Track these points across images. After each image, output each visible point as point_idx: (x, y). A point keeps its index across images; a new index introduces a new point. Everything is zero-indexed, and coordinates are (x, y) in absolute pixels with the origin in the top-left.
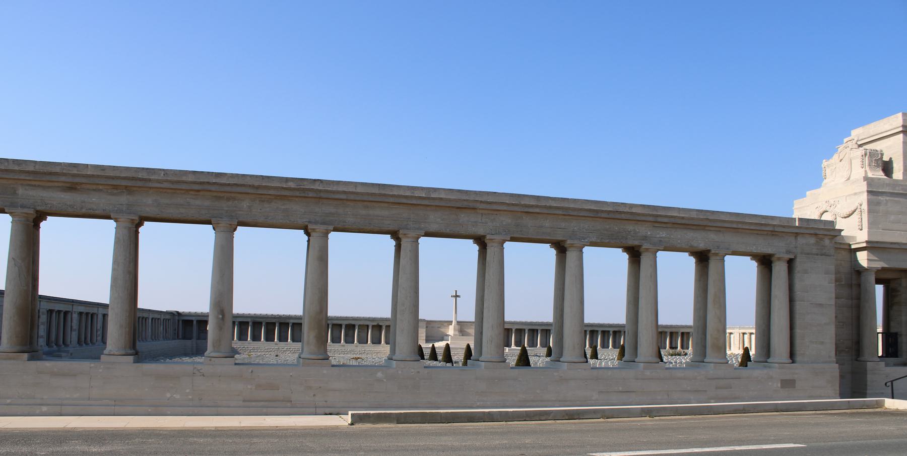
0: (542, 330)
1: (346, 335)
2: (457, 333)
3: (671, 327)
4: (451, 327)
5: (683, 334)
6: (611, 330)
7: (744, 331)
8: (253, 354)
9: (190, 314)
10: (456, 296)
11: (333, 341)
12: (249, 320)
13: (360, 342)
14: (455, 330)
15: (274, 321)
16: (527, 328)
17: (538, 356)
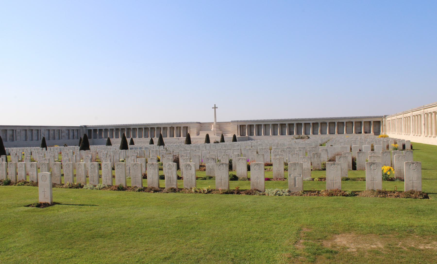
5: (177, 127)
9: (90, 127)
12: (113, 128)
14: (214, 127)
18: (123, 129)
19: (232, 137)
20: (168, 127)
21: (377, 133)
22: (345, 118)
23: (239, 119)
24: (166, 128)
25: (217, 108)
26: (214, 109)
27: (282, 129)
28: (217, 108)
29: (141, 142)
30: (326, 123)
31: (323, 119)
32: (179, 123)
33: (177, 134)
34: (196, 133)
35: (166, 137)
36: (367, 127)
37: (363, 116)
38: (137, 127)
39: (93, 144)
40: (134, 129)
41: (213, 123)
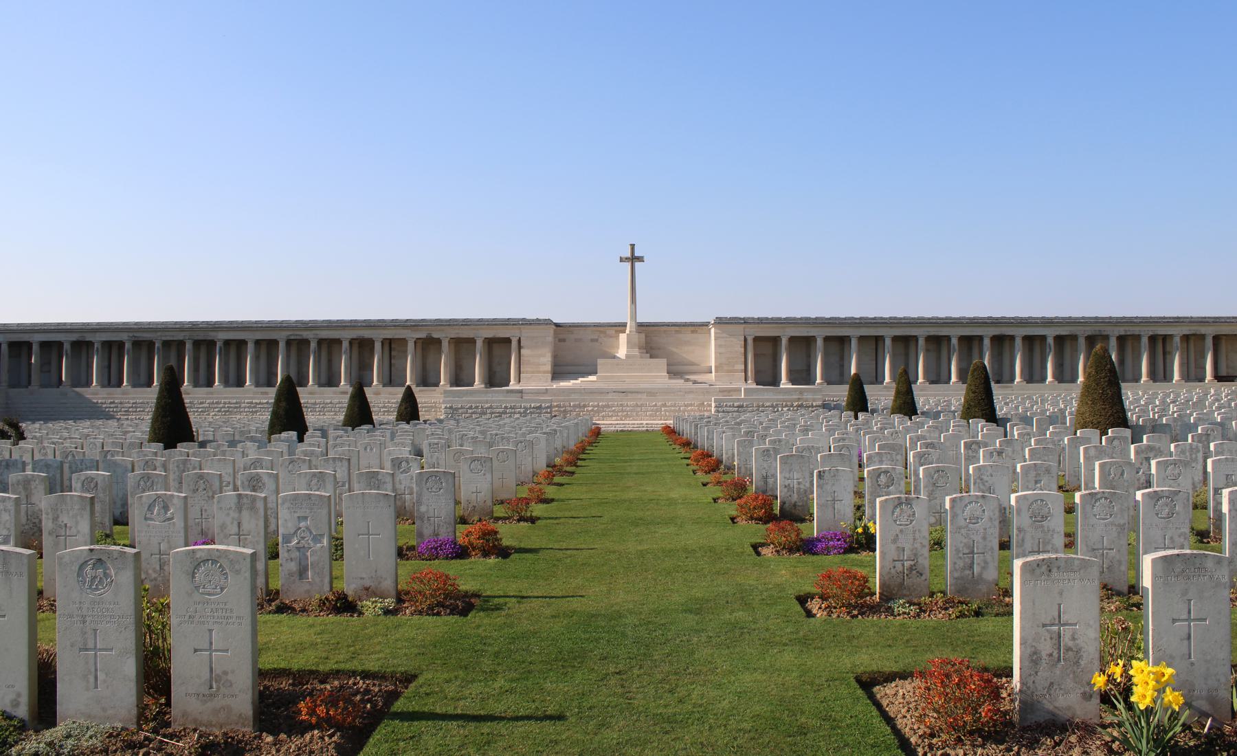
0: (862, 339)
1: (1185, 365)
2: (636, 352)
3: (1216, 321)
4: (623, 338)
5: (1153, 339)
6: (1050, 333)
8: (836, 420)
10: (634, 259)
11: (196, 383)
12: (124, 337)
13: (135, 384)
14: (630, 344)
15: (180, 336)
16: (819, 333)
17: (324, 404)
18: (970, 342)
21: (496, 379)
22: (1178, 321)
25: (640, 259)
26: (628, 265)
28: (640, 259)
29: (229, 410)
31: (1097, 321)
32: (466, 323)
33: (255, 372)
34: (549, 368)
35: (1137, 379)
38: (65, 338)
39: (48, 415)
41: (625, 325)
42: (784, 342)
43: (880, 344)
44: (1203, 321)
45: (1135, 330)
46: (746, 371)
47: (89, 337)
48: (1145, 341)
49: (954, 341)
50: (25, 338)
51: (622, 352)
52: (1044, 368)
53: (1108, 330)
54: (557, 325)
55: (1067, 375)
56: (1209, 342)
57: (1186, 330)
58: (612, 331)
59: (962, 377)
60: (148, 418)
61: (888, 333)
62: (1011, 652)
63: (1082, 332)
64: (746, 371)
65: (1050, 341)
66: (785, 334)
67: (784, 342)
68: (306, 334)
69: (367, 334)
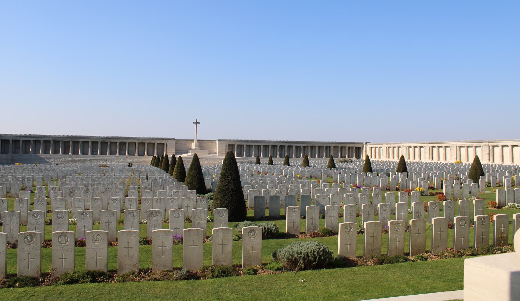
0: (255, 146)
2: (197, 148)
3: (342, 143)
4: (193, 144)
7: (431, 145)
10: (197, 123)
11: (311, 157)
12: (51, 139)
14: (196, 145)
15: (69, 140)
19: (192, 157)
20: (99, 141)
22: (332, 143)
23: (228, 139)
24: (330, 147)
25: (199, 123)
26: (195, 125)
27: (55, 146)
28: (199, 123)
30: (79, 142)
31: (313, 142)
32: (153, 139)
35: (292, 157)
36: (151, 149)
37: (292, 140)
40: (281, 147)
42: (236, 146)
43: (276, 149)
44: (338, 143)
45: (322, 145)
46: (489, 154)
47: (39, 139)
48: (324, 148)
49: (278, 147)
50: (18, 139)
51: (193, 147)
52: (300, 154)
53: (316, 145)
54: (177, 140)
55: (321, 156)
56: (340, 149)
57: (334, 145)
58: (190, 142)
59: (303, 156)
60: (284, 240)
61: (262, 144)
62: (337, 246)
63: (310, 145)
64: (489, 154)
65: (302, 147)
66: (236, 144)
67: (156, 145)
68: (107, 140)
69: (124, 141)
